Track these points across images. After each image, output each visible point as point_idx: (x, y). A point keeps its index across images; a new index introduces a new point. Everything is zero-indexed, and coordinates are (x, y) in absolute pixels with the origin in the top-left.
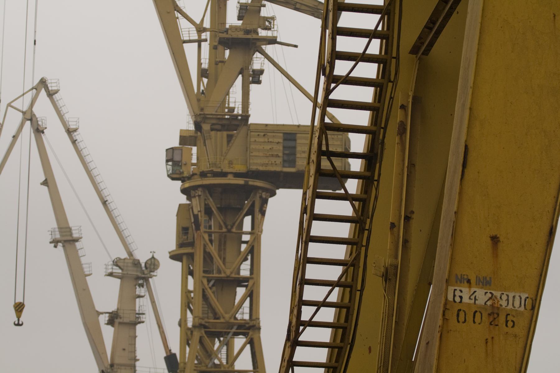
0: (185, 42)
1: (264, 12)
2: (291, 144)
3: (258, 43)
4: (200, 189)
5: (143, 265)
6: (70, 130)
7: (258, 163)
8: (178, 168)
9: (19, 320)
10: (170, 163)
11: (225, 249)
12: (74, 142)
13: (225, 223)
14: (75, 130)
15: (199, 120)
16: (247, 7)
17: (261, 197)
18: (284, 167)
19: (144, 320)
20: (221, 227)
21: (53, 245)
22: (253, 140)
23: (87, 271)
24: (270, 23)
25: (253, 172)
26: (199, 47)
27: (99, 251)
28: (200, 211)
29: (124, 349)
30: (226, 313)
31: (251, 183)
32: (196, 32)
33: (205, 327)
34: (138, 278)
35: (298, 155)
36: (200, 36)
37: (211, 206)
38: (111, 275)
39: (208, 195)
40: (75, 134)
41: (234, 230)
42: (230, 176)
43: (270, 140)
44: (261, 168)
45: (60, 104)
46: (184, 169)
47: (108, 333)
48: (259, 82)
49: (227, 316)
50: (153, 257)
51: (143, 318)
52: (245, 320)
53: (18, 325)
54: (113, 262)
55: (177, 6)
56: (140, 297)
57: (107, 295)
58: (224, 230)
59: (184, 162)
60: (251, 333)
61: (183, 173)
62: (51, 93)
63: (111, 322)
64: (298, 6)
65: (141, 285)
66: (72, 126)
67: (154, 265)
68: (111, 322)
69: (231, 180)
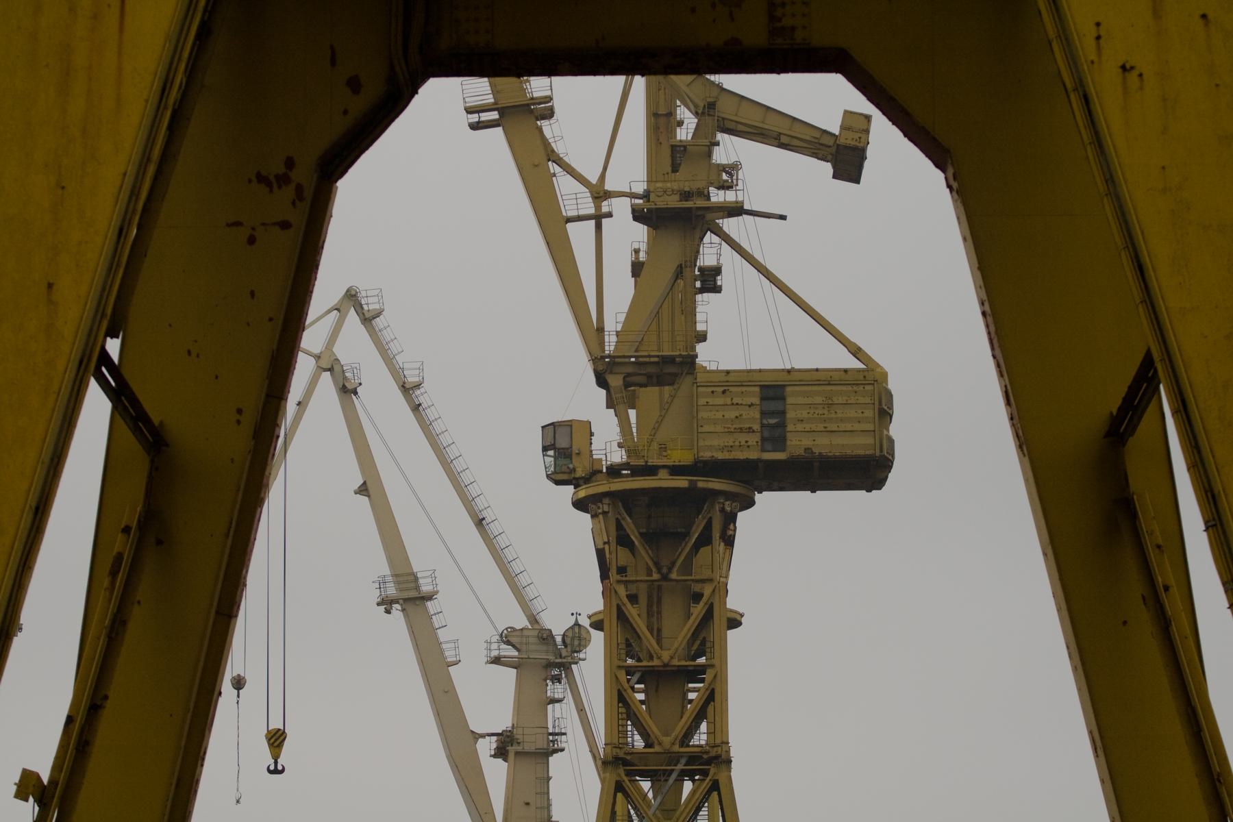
0: (569, 220)
1: (721, 156)
2: (773, 406)
3: (709, 216)
4: (606, 501)
5: (559, 639)
6: (407, 386)
7: (715, 447)
8: (566, 461)
9: (276, 763)
10: (551, 453)
11: (659, 613)
12: (416, 408)
13: (657, 564)
14: (418, 386)
15: (600, 368)
16: (685, 147)
17: (722, 510)
18: (763, 450)
19: (563, 745)
20: (649, 573)
21: (382, 608)
22: (702, 401)
23: (450, 655)
24: (731, 175)
25: (705, 463)
26: (599, 227)
27: (473, 616)
28: (608, 543)
29: (528, 804)
30: (667, 735)
31: (701, 485)
32: (590, 200)
33: (625, 763)
34: (549, 665)
35: (790, 427)
36: (598, 207)
37: (629, 531)
38: (497, 661)
39: (623, 511)
40: (418, 392)
41: (674, 576)
42: (663, 474)
43: (735, 401)
44: (720, 456)
45: (387, 335)
46: (576, 462)
47: (496, 774)
48: (717, 289)
49: (667, 741)
50: (576, 624)
51: (563, 742)
52: (701, 746)
53: (276, 771)
54: (501, 635)
55: (553, 151)
56: (554, 701)
57: (490, 700)
58: (656, 576)
59: (575, 450)
60: (712, 770)
61: (574, 470)
62: (367, 315)
63: (501, 753)
64: (784, 140)
65: (557, 679)
66: (412, 379)
67: (580, 638)
68: (501, 753)
69: (664, 481)
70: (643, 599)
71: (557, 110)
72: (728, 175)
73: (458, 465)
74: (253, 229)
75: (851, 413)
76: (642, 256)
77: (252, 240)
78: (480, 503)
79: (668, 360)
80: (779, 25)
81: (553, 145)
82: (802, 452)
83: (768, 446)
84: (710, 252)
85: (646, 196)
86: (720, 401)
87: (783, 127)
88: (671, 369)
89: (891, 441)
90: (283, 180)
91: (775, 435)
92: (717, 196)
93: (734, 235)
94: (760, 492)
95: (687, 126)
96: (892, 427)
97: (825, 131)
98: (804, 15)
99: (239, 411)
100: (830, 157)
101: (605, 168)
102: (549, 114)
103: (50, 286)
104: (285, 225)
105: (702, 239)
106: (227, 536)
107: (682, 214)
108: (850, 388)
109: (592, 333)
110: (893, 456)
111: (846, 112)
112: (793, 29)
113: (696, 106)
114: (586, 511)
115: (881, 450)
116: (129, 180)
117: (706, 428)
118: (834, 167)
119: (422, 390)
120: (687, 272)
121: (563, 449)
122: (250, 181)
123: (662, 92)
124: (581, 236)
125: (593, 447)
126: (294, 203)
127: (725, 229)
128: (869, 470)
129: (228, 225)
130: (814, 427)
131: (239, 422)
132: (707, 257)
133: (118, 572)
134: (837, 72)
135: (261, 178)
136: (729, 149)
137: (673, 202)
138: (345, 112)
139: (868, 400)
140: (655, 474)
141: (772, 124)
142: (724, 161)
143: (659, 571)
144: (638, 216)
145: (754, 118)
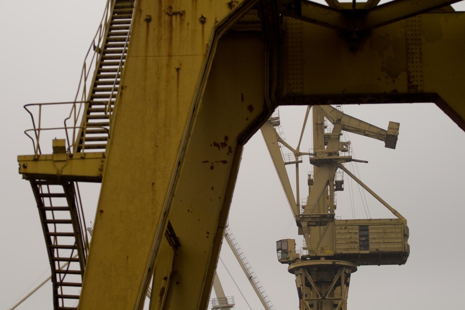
0: (286, 164)
2: (364, 233)
3: (339, 162)
4: (301, 269)
7: (342, 249)
10: (280, 251)
13: (320, 293)
15: (298, 219)
16: (329, 136)
17: (345, 273)
18: (360, 250)
20: (318, 297)
22: (337, 232)
24: (347, 146)
25: (339, 255)
26: (297, 166)
28: (302, 285)
31: (337, 263)
32: (294, 156)
35: (370, 241)
36: (297, 159)
39: (307, 273)
41: (327, 297)
42: (322, 259)
43: (349, 231)
44: (344, 252)
46: (290, 255)
48: (342, 189)
55: (280, 138)
58: (320, 298)
59: (289, 250)
61: (289, 258)
64: (367, 133)
69: (323, 262)
70: (315, 306)
71: (281, 122)
72: (345, 146)
73: (242, 257)
74: (213, 163)
75: (393, 236)
76: (312, 177)
77: (212, 168)
78: (250, 271)
79: (324, 216)
80: (411, 84)
81: (280, 135)
82: (375, 250)
83: (362, 248)
84: (339, 175)
85: (315, 154)
86: (344, 231)
87: (366, 128)
88: (325, 220)
89: (408, 246)
90: (224, 145)
91: (365, 244)
92: (342, 154)
93: (348, 169)
94: (359, 266)
95: (329, 128)
96: (408, 240)
97: (382, 129)
98: (421, 81)
99: (208, 233)
100: (384, 139)
101: (299, 144)
102: (278, 124)
103: (153, 184)
104: (225, 162)
105: (336, 170)
106: (204, 280)
107: (328, 161)
108: (393, 226)
109: (295, 206)
110: (409, 251)
111: (390, 122)
112: (417, 86)
113: (334, 120)
114: (294, 274)
115: (405, 250)
116: (182, 143)
117: (339, 242)
118: (386, 143)
119: (228, 228)
120: (331, 183)
121: (284, 250)
122: (211, 145)
123: (319, 115)
124: (290, 170)
125: (296, 249)
126: (228, 154)
127: (345, 167)
128: (399, 257)
129: (203, 162)
130: (379, 241)
131: (208, 237)
132: (338, 178)
133: (163, 294)
134: (433, 102)
135: (216, 144)
136: (346, 136)
137: (326, 157)
138: (247, 119)
139: (399, 231)
140: (320, 259)
141: (362, 127)
142: (344, 141)
143: (321, 296)
144: (312, 162)
145: (355, 125)
